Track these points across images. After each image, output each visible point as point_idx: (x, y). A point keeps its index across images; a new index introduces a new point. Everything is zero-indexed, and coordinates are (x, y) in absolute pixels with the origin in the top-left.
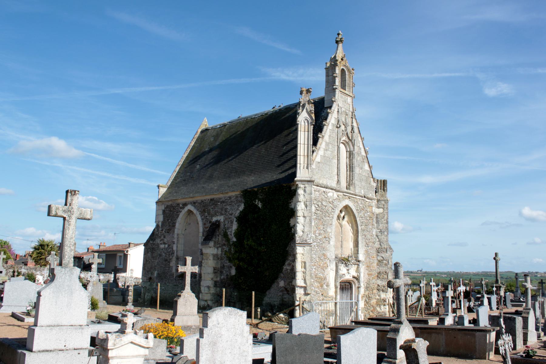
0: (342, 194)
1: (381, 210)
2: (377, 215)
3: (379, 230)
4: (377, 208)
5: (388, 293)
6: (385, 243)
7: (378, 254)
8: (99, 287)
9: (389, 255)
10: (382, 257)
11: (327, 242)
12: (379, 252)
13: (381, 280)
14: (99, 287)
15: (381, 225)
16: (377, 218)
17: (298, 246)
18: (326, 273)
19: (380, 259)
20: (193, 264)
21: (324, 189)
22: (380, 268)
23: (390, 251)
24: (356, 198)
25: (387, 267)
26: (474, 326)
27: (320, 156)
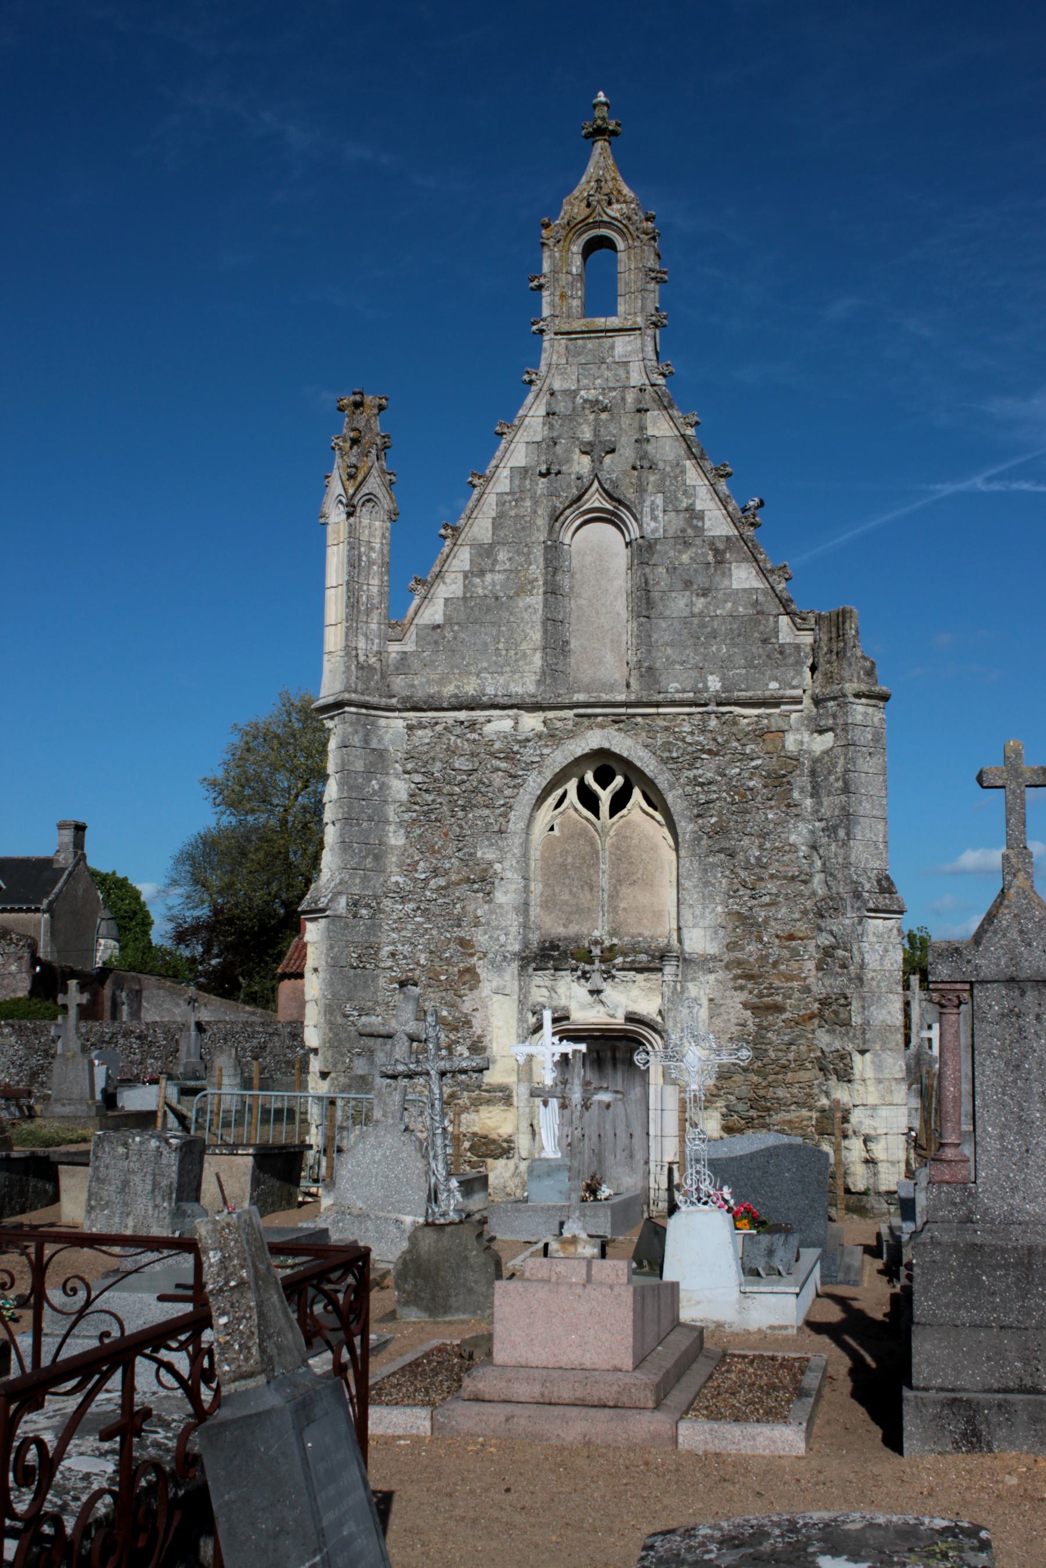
0: (570, 714)
1: (828, 740)
2: (815, 761)
3: (823, 824)
4: (815, 735)
5: (857, 1086)
6: (840, 876)
7: (819, 921)
8: (80, 1067)
9: (853, 924)
10: (831, 932)
11: (481, 895)
12: (822, 916)
13: (828, 1031)
14: (80, 1067)
15: (826, 801)
16: (813, 773)
17: (306, 919)
18: (466, 1007)
19: (827, 943)
20: (65, 991)
21: (462, 715)
22: (827, 983)
23: (856, 906)
24: (658, 714)
25: (849, 974)
26: (604, 1182)
27: (442, 601)
